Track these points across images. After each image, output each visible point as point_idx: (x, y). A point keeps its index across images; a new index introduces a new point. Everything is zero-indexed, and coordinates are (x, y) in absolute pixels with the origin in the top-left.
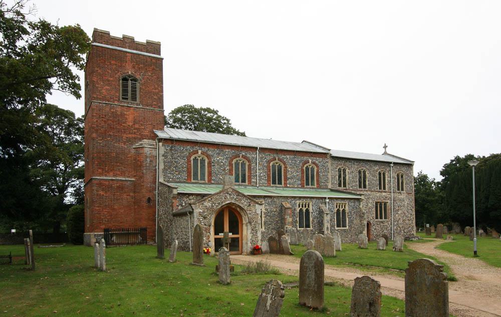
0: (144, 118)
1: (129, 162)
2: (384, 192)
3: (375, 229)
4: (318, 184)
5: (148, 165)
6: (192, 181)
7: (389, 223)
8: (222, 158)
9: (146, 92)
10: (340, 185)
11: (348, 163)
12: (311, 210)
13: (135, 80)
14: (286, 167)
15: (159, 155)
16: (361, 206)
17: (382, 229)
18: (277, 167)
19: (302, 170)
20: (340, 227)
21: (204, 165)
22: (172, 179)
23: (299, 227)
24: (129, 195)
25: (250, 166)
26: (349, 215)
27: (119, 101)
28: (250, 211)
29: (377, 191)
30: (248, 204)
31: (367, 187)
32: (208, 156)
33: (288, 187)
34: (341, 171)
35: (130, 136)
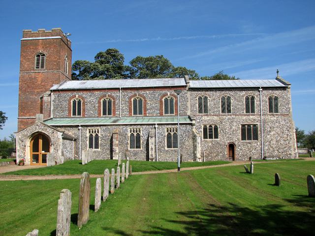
3: (241, 149)
6: (72, 116)
13: (44, 55)
14: (146, 101)
17: (249, 149)
19: (161, 101)
23: (130, 148)
27: (34, 70)
32: (83, 98)
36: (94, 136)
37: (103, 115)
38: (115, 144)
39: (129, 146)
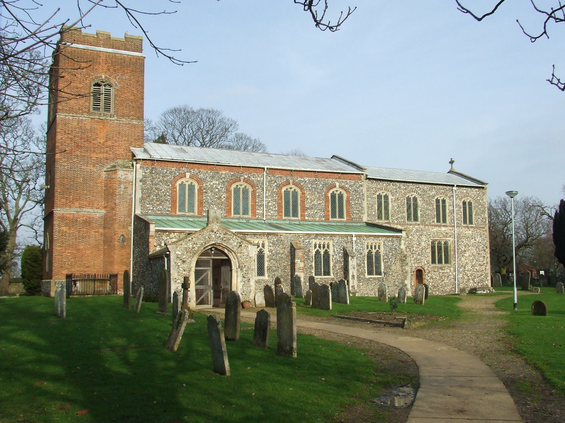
0: (119, 133)
1: (99, 189)
2: (444, 226)
4: (348, 215)
5: (122, 193)
7: (452, 269)
8: (217, 182)
9: (122, 100)
10: (380, 217)
11: (391, 186)
12: (331, 252)
14: (303, 194)
15: (135, 180)
16: (403, 247)
18: (241, 190)
19: (326, 197)
20: (373, 275)
21: (194, 192)
22: (152, 210)
24: (98, 232)
25: (254, 192)
26: (385, 259)
27: (89, 112)
28: (241, 253)
29: (432, 225)
30: (239, 245)
31: (419, 219)
33: (306, 220)
34: (439, 202)
35: (101, 156)
36: (322, 253)
37: (235, 214)
38: (299, 269)
39: (313, 271)
